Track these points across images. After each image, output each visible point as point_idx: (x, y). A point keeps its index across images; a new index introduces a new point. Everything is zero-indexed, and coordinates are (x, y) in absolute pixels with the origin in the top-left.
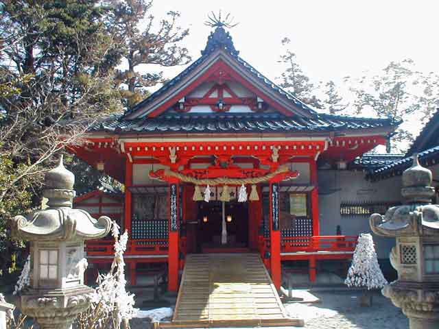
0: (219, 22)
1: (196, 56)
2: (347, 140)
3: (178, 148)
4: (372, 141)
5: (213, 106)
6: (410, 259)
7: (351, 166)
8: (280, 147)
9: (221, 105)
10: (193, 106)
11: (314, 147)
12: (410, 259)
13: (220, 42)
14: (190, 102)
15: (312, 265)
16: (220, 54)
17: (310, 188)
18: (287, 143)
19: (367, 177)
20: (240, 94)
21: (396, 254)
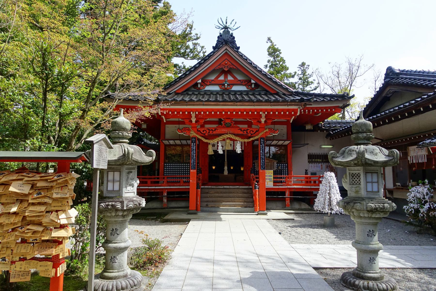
0: (226, 26)
1: (209, 50)
2: (313, 109)
3: (197, 113)
4: (331, 110)
5: (221, 86)
6: (356, 182)
7: (317, 128)
8: (266, 113)
9: (226, 85)
10: (207, 85)
11: (290, 113)
12: (356, 182)
13: (226, 40)
14: (205, 83)
15: (287, 195)
16: (226, 49)
17: (287, 143)
18: (272, 110)
19: (327, 137)
20: (239, 78)
21: (346, 179)
